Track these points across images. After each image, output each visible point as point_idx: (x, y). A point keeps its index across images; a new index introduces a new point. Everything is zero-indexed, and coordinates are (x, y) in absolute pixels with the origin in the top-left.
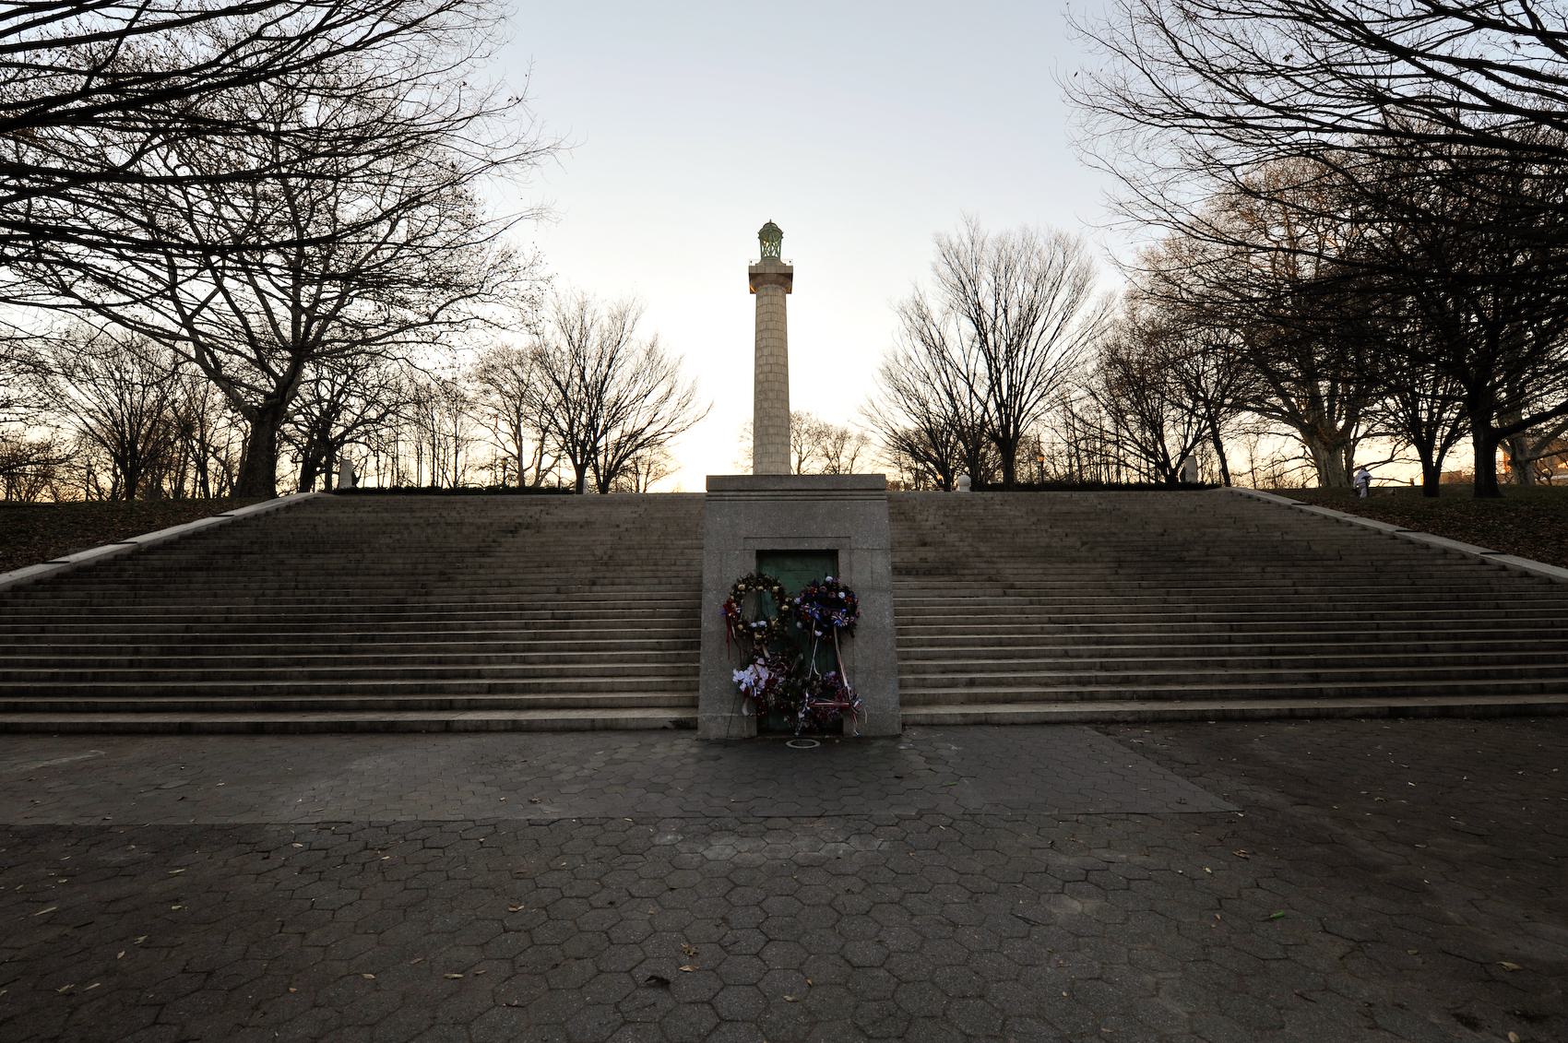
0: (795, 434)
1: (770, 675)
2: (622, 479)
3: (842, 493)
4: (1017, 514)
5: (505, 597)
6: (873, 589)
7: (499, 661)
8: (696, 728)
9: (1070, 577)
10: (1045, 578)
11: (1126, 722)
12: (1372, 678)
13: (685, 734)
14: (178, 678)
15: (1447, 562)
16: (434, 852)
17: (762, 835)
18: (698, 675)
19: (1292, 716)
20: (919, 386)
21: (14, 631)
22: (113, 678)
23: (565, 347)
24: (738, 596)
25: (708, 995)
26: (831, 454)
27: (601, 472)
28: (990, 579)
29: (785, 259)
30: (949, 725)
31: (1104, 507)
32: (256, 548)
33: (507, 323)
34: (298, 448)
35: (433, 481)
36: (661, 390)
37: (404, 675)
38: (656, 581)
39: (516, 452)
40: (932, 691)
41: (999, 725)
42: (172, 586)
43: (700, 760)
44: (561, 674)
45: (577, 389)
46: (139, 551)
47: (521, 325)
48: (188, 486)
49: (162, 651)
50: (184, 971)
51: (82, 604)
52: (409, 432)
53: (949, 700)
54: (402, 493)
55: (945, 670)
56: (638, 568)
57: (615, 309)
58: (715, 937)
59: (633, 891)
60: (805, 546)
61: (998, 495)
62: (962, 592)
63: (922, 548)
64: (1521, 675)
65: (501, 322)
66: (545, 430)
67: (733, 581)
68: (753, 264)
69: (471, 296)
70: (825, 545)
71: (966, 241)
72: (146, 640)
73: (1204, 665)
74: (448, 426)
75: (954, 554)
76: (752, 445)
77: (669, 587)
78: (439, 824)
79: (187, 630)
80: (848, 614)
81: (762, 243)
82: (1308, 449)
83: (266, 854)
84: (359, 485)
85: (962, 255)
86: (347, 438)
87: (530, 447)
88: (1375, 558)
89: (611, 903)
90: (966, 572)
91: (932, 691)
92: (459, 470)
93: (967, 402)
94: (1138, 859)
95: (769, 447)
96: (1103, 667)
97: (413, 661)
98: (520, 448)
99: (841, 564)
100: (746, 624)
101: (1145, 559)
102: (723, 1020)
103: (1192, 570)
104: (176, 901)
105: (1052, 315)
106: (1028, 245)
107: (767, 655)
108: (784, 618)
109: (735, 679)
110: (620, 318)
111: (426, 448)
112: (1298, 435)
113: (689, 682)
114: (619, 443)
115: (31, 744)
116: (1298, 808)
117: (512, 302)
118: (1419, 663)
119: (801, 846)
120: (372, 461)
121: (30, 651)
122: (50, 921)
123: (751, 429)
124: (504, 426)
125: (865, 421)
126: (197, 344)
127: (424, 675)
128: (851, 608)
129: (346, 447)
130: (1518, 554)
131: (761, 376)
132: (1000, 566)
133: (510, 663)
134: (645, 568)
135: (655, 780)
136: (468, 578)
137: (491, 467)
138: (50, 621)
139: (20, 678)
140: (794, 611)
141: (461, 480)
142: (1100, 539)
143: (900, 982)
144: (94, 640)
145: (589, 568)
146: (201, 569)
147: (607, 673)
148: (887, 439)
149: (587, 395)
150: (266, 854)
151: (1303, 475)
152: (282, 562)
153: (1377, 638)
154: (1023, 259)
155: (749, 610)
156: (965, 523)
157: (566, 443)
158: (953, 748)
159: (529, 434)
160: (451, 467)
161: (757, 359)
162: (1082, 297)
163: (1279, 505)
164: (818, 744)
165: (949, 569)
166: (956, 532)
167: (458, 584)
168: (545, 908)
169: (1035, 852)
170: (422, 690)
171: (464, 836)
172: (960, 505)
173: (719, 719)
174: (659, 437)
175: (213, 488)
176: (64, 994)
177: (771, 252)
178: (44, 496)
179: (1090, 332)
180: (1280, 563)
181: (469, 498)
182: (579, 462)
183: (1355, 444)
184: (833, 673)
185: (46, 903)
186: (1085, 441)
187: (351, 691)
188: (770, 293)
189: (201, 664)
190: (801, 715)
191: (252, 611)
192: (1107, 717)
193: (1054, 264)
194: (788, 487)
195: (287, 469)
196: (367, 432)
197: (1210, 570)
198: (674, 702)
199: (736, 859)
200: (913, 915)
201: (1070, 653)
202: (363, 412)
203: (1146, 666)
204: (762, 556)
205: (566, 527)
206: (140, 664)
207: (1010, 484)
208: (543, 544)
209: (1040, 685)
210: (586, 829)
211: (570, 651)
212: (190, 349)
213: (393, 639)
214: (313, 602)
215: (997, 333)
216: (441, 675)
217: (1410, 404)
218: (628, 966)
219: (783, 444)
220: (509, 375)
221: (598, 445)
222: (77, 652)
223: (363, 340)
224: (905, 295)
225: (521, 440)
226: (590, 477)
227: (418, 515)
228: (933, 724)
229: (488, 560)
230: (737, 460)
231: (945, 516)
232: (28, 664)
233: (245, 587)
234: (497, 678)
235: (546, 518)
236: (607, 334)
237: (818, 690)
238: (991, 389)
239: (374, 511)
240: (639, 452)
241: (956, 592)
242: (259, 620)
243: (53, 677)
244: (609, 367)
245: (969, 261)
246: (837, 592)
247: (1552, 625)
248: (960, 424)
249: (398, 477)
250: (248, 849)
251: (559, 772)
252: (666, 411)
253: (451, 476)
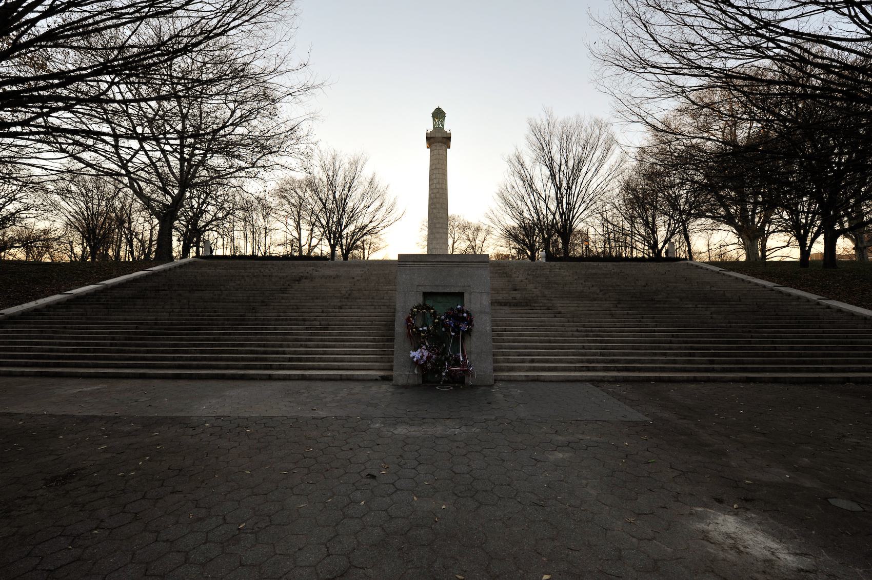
0: (451, 227)
2: (355, 252)
4: (568, 274)
5: (295, 314)
7: (294, 346)
8: (392, 380)
9: (591, 308)
10: (578, 309)
11: (609, 381)
12: (743, 363)
13: (387, 382)
14: (135, 352)
15: (798, 303)
16: (270, 429)
17: (420, 425)
18: (393, 355)
19: (695, 380)
20: (519, 203)
21: (51, 328)
22: (103, 351)
23: (325, 179)
24: (413, 315)
25: (392, 481)
26: (471, 239)
27: (344, 247)
28: (548, 309)
29: (446, 128)
30: (518, 381)
31: (615, 271)
32: (166, 287)
33: (294, 167)
34: (181, 233)
35: (253, 252)
36: (377, 204)
37: (247, 352)
38: (373, 307)
39: (297, 236)
40: (512, 365)
41: (544, 381)
42: (126, 306)
43: (393, 394)
44: (325, 353)
45: (331, 202)
46: (107, 289)
47: (301, 168)
48: (122, 253)
49: (126, 339)
50: (169, 469)
51: (82, 315)
52: (239, 225)
53: (520, 369)
54: (236, 259)
55: (520, 354)
56: (364, 300)
57: (352, 159)
58: (397, 462)
59: (361, 445)
60: (447, 290)
61: (558, 264)
62: (532, 315)
63: (514, 292)
64: (822, 363)
65: (290, 166)
66: (313, 225)
67: (411, 307)
68: (429, 132)
69: (274, 152)
70: (457, 290)
71: (545, 122)
72: (117, 333)
73: (655, 354)
74: (261, 222)
75: (531, 295)
76: (427, 234)
77: (380, 310)
78: (271, 418)
79: (137, 328)
80: (468, 324)
81: (434, 120)
82: (740, 239)
83: (194, 428)
84: (214, 254)
85: (542, 131)
86: (207, 228)
87: (305, 234)
88: (759, 300)
89: (351, 449)
90: (536, 305)
91: (512, 365)
92: (267, 246)
93: (544, 212)
94: (595, 439)
95: (437, 235)
96: (602, 354)
97: (251, 346)
98: (300, 234)
99: (465, 300)
100: (417, 328)
101: (634, 299)
102: (398, 490)
103: (658, 305)
104: (158, 445)
105: (592, 163)
106: (579, 125)
107: (427, 344)
108: (436, 326)
109: (411, 356)
110: (355, 164)
111: (249, 234)
112: (735, 231)
113: (389, 358)
114: (353, 233)
115: (70, 382)
116: (680, 421)
117: (296, 155)
118: (769, 355)
119: (439, 430)
120: (220, 241)
121: (61, 338)
122: (105, 451)
123: (426, 224)
124: (291, 222)
125: (488, 222)
126: (130, 178)
127: (257, 352)
128: (470, 322)
129: (206, 233)
130: (838, 300)
131: (432, 195)
132: (554, 302)
133: (299, 347)
134: (367, 300)
135: (372, 402)
136: (276, 304)
137: (284, 244)
138: (68, 323)
139: (58, 351)
141: (268, 251)
142: (610, 288)
143: (475, 479)
144: (91, 333)
145: (339, 300)
146: (140, 298)
147: (348, 353)
148: (501, 232)
149: (337, 206)
150: (194, 428)
151: (736, 252)
152: (180, 295)
153: (750, 342)
154: (576, 133)
155: (419, 322)
156: (538, 279)
157: (325, 231)
158: (519, 391)
159: (305, 227)
160: (263, 244)
161: (430, 185)
162: (610, 153)
163: (712, 271)
164: (452, 388)
165: (527, 303)
166: (533, 283)
167: (271, 307)
168: (322, 450)
169: (547, 435)
170: (256, 359)
171: (283, 422)
172: (537, 269)
174: (376, 230)
175: (136, 254)
176: (121, 476)
178: (46, 259)
179: (618, 169)
180: (706, 303)
181: (275, 262)
182: (332, 243)
183: (767, 237)
185: (101, 445)
186: (613, 235)
187: (221, 359)
189: (145, 345)
190: (444, 374)
191: (168, 320)
192: (599, 378)
193: (594, 136)
194: (439, 260)
195: (177, 246)
196: (217, 226)
197: (667, 306)
198: (381, 368)
199: (408, 434)
200: (485, 457)
201: (585, 347)
202: (216, 214)
203: (624, 354)
204: (426, 295)
205: (326, 278)
206: (116, 345)
207: (567, 258)
208: (314, 287)
209: (568, 363)
210: (339, 421)
211: (329, 342)
212: (126, 180)
213: (240, 334)
214: (198, 315)
215: (561, 173)
216: (265, 352)
217: (794, 213)
218: (358, 471)
219: (444, 233)
220: (294, 194)
221: (343, 234)
222: (83, 339)
223: (219, 176)
224: (511, 152)
225: (300, 229)
226: (338, 251)
227: (249, 271)
228: (510, 380)
229: (286, 295)
230: (418, 245)
231: (528, 274)
232: (61, 344)
233: (163, 308)
234: (293, 354)
235: (315, 273)
236: (347, 173)
237: (452, 362)
238: (558, 206)
239: (225, 269)
240: (365, 238)
241: (530, 315)
242: (172, 324)
243: (74, 351)
244: (349, 191)
245: (546, 134)
246: (463, 314)
247: (847, 337)
248: (541, 225)
249: (234, 249)
250: (185, 426)
251: (325, 397)
252: (379, 216)
253: (262, 249)
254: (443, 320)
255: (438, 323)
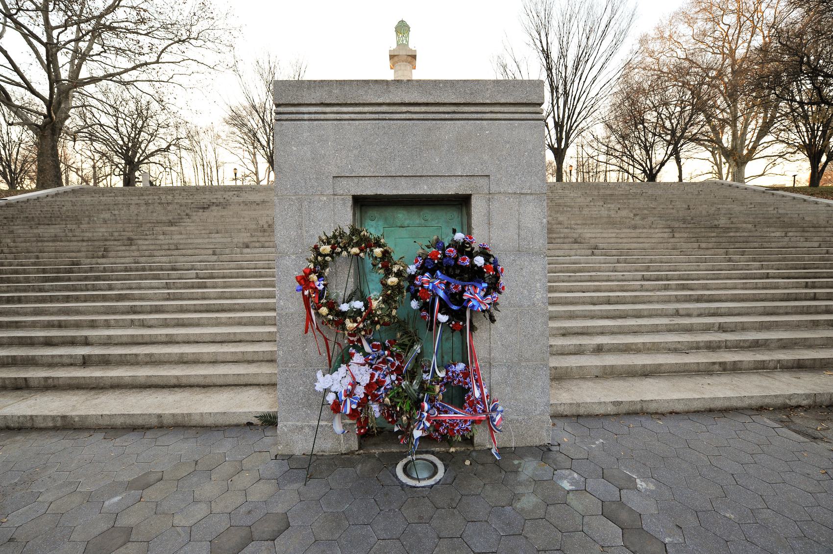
1: (372, 376)
3: (479, 109)
6: (519, 251)
24: (320, 265)
29: (411, 46)
60: (424, 189)
70: (451, 188)
81: (397, 35)
100: (332, 306)
109: (319, 387)
132: (580, 231)
140: (406, 284)
173: (307, 430)
177: (403, 41)
184: (461, 366)
188: (403, 68)
191: (34, 264)
194: (398, 100)
201: (681, 312)
204: (362, 203)
225: (257, 163)
254: (412, 278)
255: (398, 288)
